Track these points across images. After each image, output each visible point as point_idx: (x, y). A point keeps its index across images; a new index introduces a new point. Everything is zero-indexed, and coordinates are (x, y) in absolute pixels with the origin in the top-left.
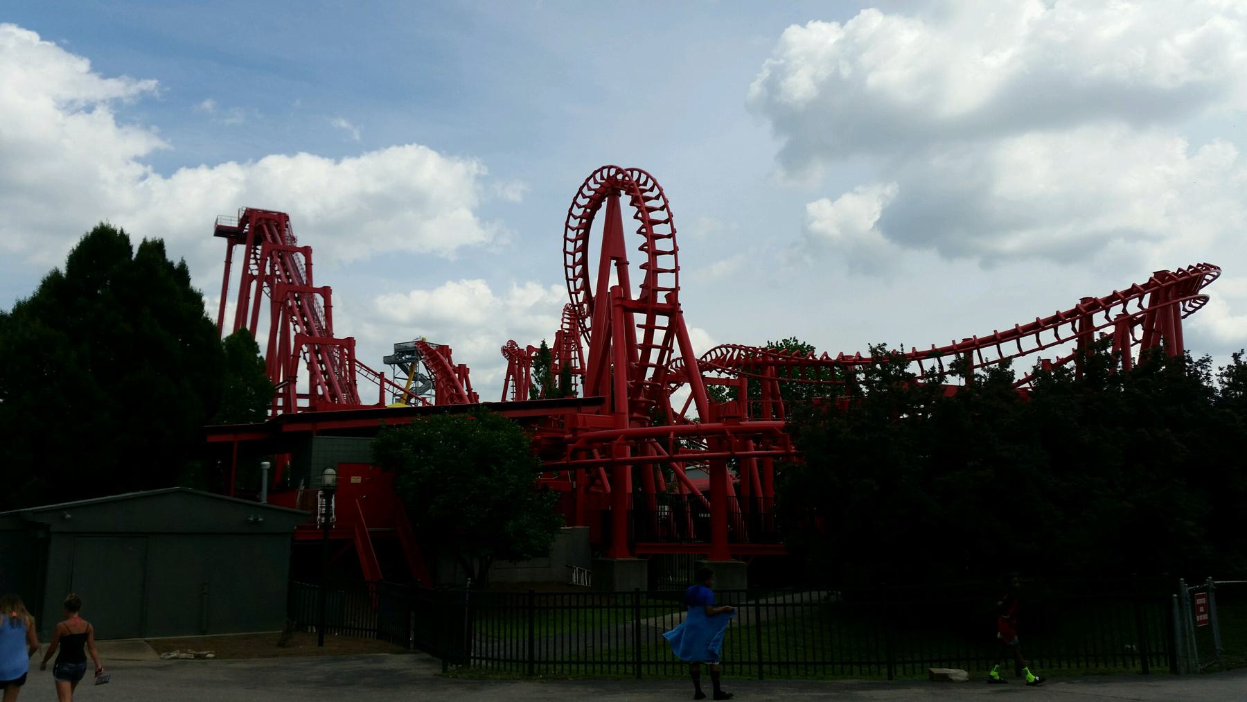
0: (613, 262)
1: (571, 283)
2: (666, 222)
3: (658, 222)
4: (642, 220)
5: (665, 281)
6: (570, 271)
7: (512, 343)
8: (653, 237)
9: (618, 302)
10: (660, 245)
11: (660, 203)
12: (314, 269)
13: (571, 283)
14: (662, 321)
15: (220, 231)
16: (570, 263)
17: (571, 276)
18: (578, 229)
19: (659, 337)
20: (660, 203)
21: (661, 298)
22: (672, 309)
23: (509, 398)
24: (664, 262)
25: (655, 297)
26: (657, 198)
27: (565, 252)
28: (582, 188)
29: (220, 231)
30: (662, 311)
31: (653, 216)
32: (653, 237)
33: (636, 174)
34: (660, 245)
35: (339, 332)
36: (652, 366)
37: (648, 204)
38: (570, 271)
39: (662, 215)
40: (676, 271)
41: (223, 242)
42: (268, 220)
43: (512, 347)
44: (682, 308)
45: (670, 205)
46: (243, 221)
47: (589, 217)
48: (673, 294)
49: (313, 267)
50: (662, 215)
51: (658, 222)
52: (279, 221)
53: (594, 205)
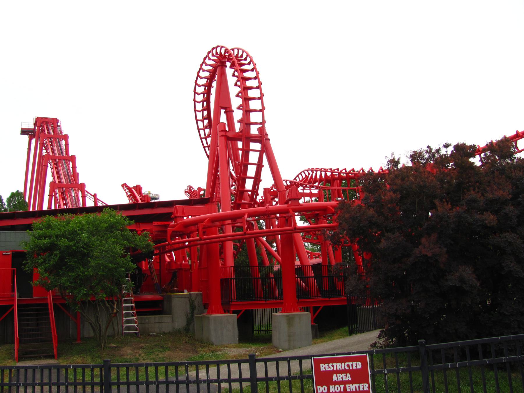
0: (223, 111)
1: (204, 140)
2: (255, 78)
3: (251, 88)
4: (237, 77)
5: (255, 117)
6: (202, 132)
7: (191, 187)
8: (246, 89)
9: (223, 133)
10: (251, 93)
11: (251, 67)
12: (70, 147)
13: (204, 140)
14: (255, 146)
15: (24, 132)
16: (201, 126)
17: (203, 136)
18: (203, 101)
19: (253, 157)
20: (251, 67)
21: (254, 130)
22: (263, 138)
23: (53, 207)
24: (254, 105)
25: (249, 130)
26: (249, 64)
27: (197, 120)
28: (202, 65)
29: (24, 132)
30: (255, 139)
31: (246, 75)
32: (246, 89)
33: (236, 51)
34: (251, 93)
35: (80, 181)
36: (240, 149)
37: (243, 68)
38: (202, 132)
39: (252, 74)
40: (262, 110)
41: (26, 137)
42: (48, 122)
43: (190, 190)
44: (269, 137)
45: (257, 67)
46: (35, 125)
47: (209, 86)
48: (262, 130)
49: (70, 146)
50: (252, 74)
51: (251, 88)
52: (54, 123)
53: (210, 79)
